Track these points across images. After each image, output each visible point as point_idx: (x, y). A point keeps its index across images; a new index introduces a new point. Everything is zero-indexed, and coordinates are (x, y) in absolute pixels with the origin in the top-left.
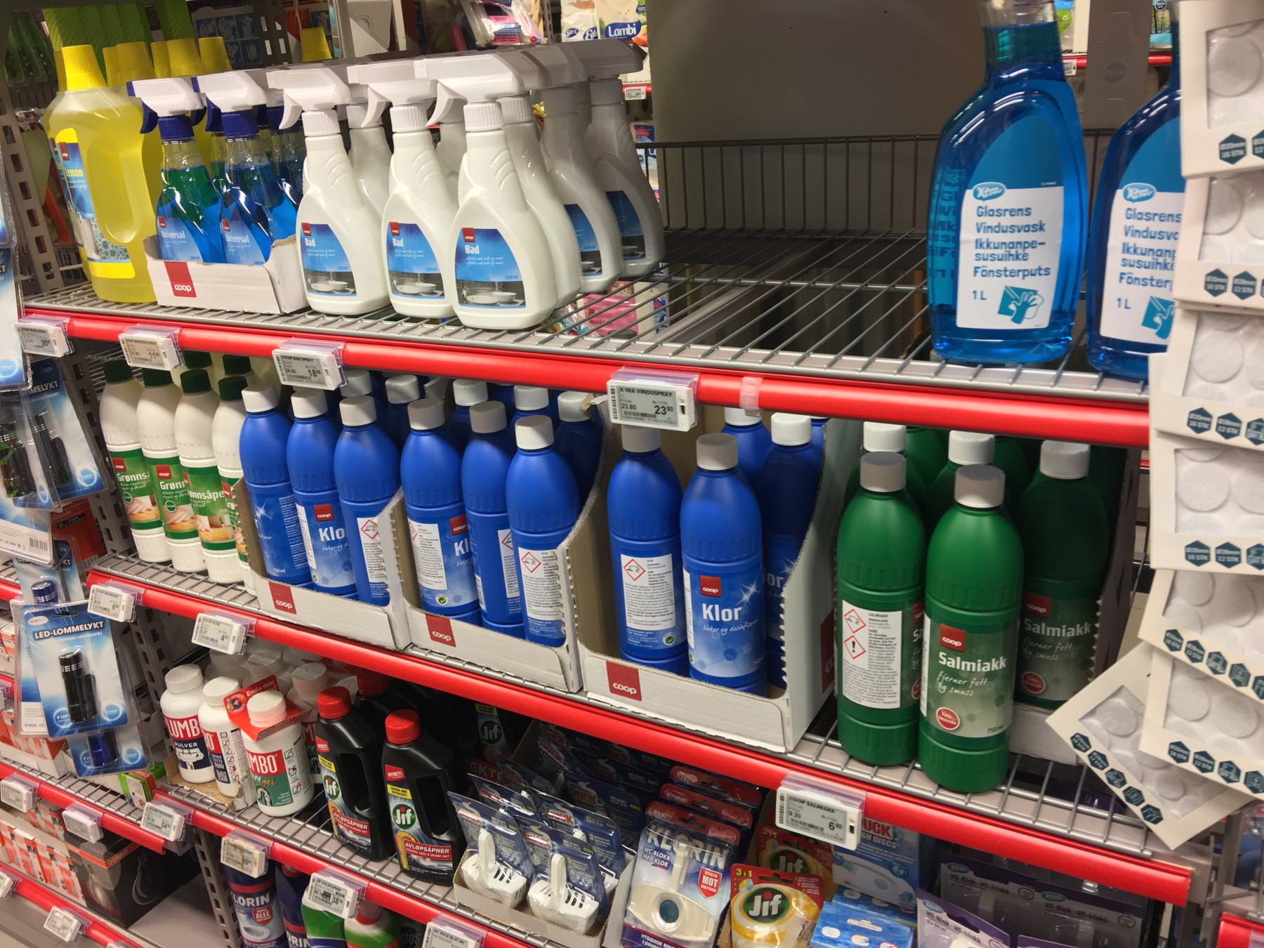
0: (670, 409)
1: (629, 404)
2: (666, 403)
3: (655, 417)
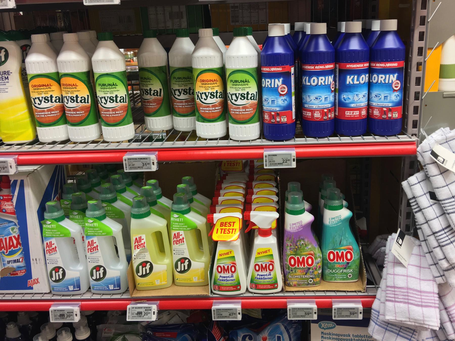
0: (6, 167)
1: (272, 161)
2: (4, 165)
3: (283, 164)
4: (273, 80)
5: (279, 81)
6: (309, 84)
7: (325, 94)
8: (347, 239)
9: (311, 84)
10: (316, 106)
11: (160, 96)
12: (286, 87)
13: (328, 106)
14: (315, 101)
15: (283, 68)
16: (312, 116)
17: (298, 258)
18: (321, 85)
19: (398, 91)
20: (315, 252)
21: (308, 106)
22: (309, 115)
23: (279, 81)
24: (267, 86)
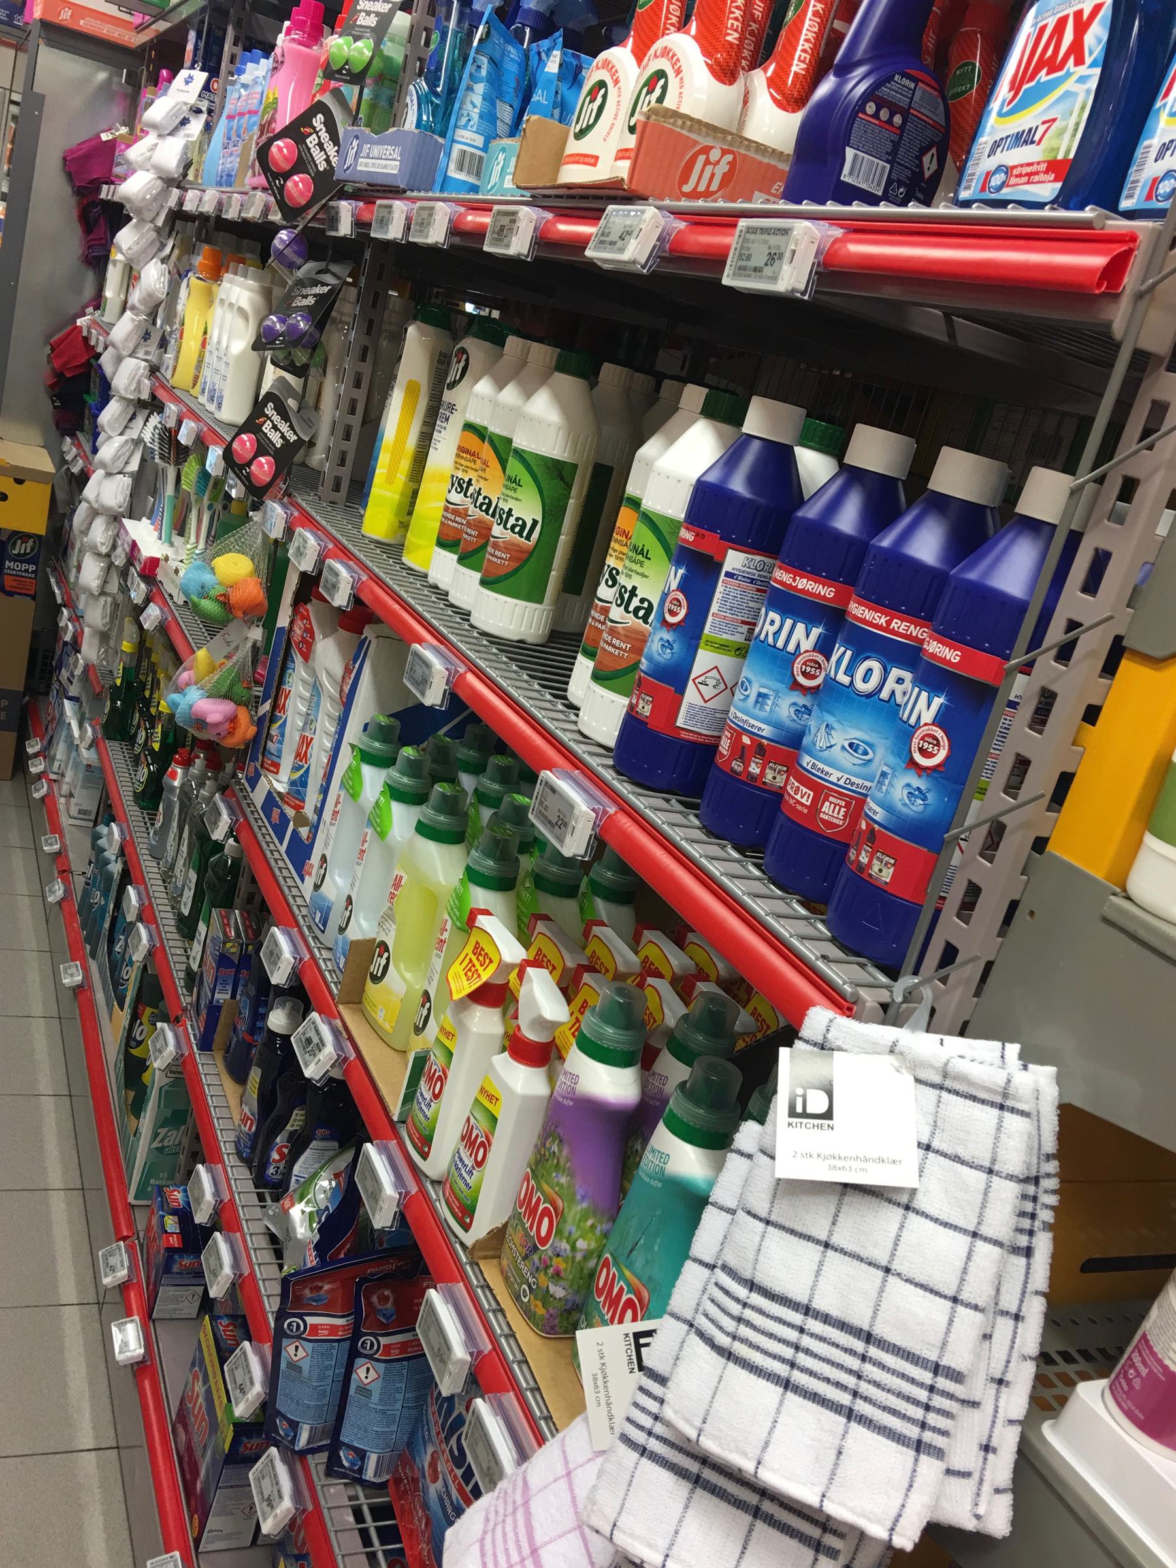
4: (789, 623)
5: (808, 637)
6: (845, 680)
7: (764, 681)
8: (649, 1257)
9: (852, 682)
10: (840, 774)
11: (528, 538)
12: (944, 742)
13: (759, 729)
14: (846, 754)
15: (697, 535)
16: (815, 807)
17: (539, 1199)
18: (888, 702)
19: (924, 774)
20: (566, 1210)
21: (814, 765)
22: (804, 801)
23: (808, 637)
24: (762, 637)
